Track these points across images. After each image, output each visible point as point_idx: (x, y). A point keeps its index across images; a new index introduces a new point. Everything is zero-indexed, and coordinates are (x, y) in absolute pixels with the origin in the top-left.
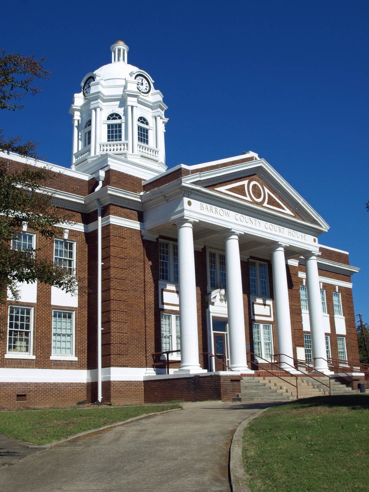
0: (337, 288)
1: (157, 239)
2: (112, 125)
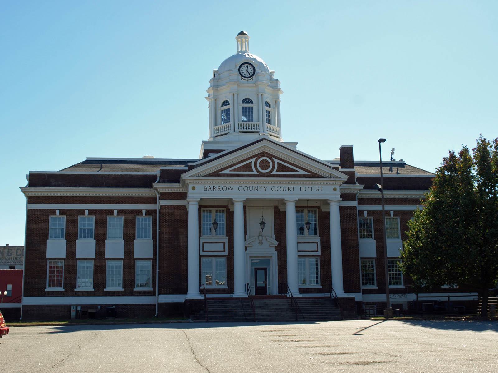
2: (246, 107)
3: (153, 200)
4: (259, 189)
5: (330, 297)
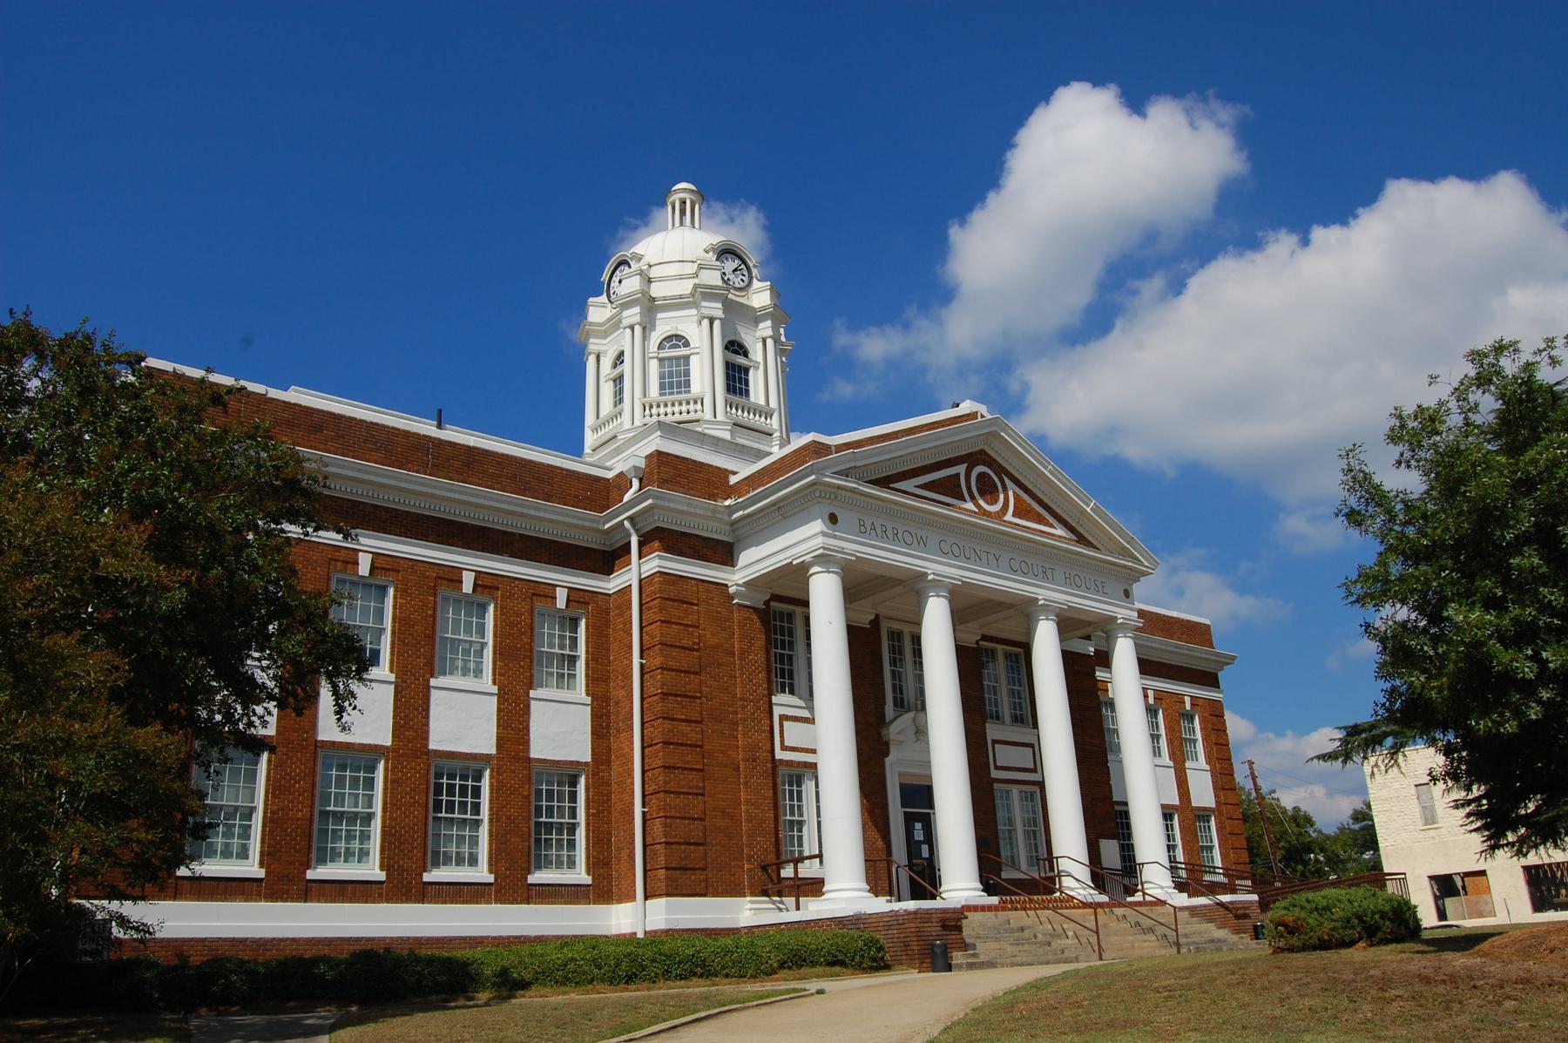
0: (1187, 700)
1: (767, 603)
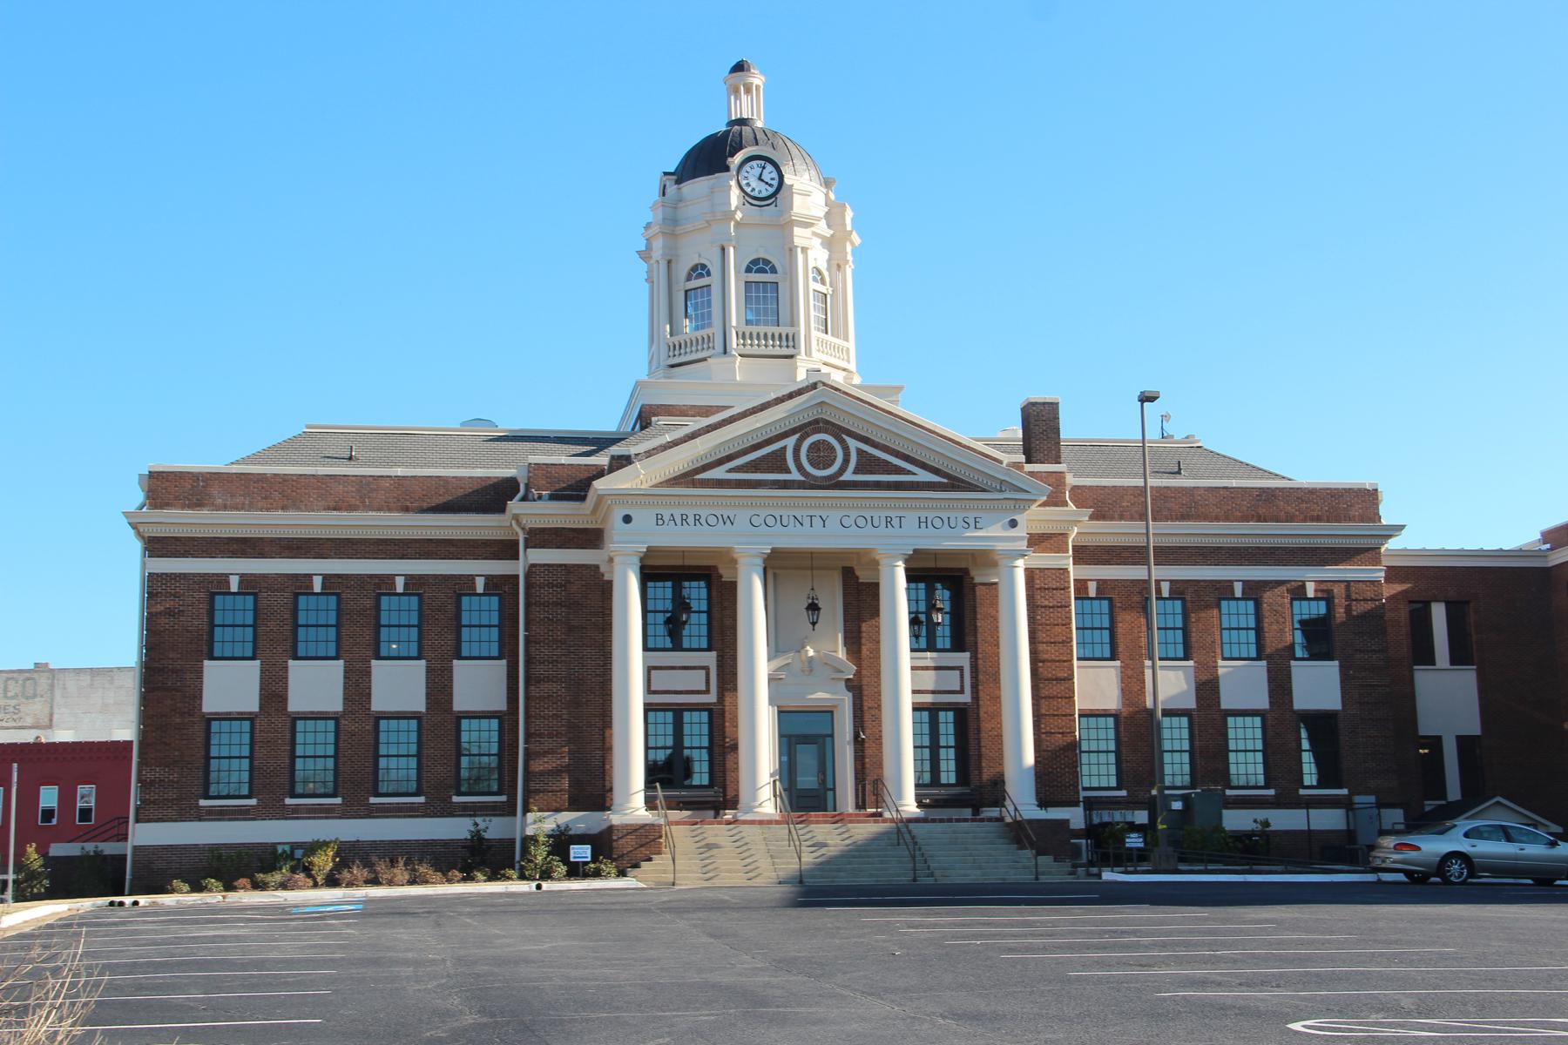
3: (507, 550)
4: (807, 521)
5: (1000, 819)
